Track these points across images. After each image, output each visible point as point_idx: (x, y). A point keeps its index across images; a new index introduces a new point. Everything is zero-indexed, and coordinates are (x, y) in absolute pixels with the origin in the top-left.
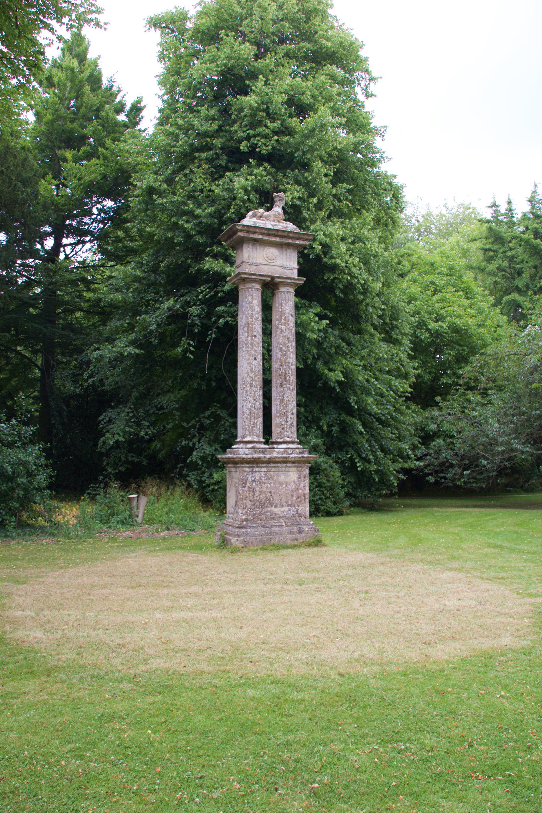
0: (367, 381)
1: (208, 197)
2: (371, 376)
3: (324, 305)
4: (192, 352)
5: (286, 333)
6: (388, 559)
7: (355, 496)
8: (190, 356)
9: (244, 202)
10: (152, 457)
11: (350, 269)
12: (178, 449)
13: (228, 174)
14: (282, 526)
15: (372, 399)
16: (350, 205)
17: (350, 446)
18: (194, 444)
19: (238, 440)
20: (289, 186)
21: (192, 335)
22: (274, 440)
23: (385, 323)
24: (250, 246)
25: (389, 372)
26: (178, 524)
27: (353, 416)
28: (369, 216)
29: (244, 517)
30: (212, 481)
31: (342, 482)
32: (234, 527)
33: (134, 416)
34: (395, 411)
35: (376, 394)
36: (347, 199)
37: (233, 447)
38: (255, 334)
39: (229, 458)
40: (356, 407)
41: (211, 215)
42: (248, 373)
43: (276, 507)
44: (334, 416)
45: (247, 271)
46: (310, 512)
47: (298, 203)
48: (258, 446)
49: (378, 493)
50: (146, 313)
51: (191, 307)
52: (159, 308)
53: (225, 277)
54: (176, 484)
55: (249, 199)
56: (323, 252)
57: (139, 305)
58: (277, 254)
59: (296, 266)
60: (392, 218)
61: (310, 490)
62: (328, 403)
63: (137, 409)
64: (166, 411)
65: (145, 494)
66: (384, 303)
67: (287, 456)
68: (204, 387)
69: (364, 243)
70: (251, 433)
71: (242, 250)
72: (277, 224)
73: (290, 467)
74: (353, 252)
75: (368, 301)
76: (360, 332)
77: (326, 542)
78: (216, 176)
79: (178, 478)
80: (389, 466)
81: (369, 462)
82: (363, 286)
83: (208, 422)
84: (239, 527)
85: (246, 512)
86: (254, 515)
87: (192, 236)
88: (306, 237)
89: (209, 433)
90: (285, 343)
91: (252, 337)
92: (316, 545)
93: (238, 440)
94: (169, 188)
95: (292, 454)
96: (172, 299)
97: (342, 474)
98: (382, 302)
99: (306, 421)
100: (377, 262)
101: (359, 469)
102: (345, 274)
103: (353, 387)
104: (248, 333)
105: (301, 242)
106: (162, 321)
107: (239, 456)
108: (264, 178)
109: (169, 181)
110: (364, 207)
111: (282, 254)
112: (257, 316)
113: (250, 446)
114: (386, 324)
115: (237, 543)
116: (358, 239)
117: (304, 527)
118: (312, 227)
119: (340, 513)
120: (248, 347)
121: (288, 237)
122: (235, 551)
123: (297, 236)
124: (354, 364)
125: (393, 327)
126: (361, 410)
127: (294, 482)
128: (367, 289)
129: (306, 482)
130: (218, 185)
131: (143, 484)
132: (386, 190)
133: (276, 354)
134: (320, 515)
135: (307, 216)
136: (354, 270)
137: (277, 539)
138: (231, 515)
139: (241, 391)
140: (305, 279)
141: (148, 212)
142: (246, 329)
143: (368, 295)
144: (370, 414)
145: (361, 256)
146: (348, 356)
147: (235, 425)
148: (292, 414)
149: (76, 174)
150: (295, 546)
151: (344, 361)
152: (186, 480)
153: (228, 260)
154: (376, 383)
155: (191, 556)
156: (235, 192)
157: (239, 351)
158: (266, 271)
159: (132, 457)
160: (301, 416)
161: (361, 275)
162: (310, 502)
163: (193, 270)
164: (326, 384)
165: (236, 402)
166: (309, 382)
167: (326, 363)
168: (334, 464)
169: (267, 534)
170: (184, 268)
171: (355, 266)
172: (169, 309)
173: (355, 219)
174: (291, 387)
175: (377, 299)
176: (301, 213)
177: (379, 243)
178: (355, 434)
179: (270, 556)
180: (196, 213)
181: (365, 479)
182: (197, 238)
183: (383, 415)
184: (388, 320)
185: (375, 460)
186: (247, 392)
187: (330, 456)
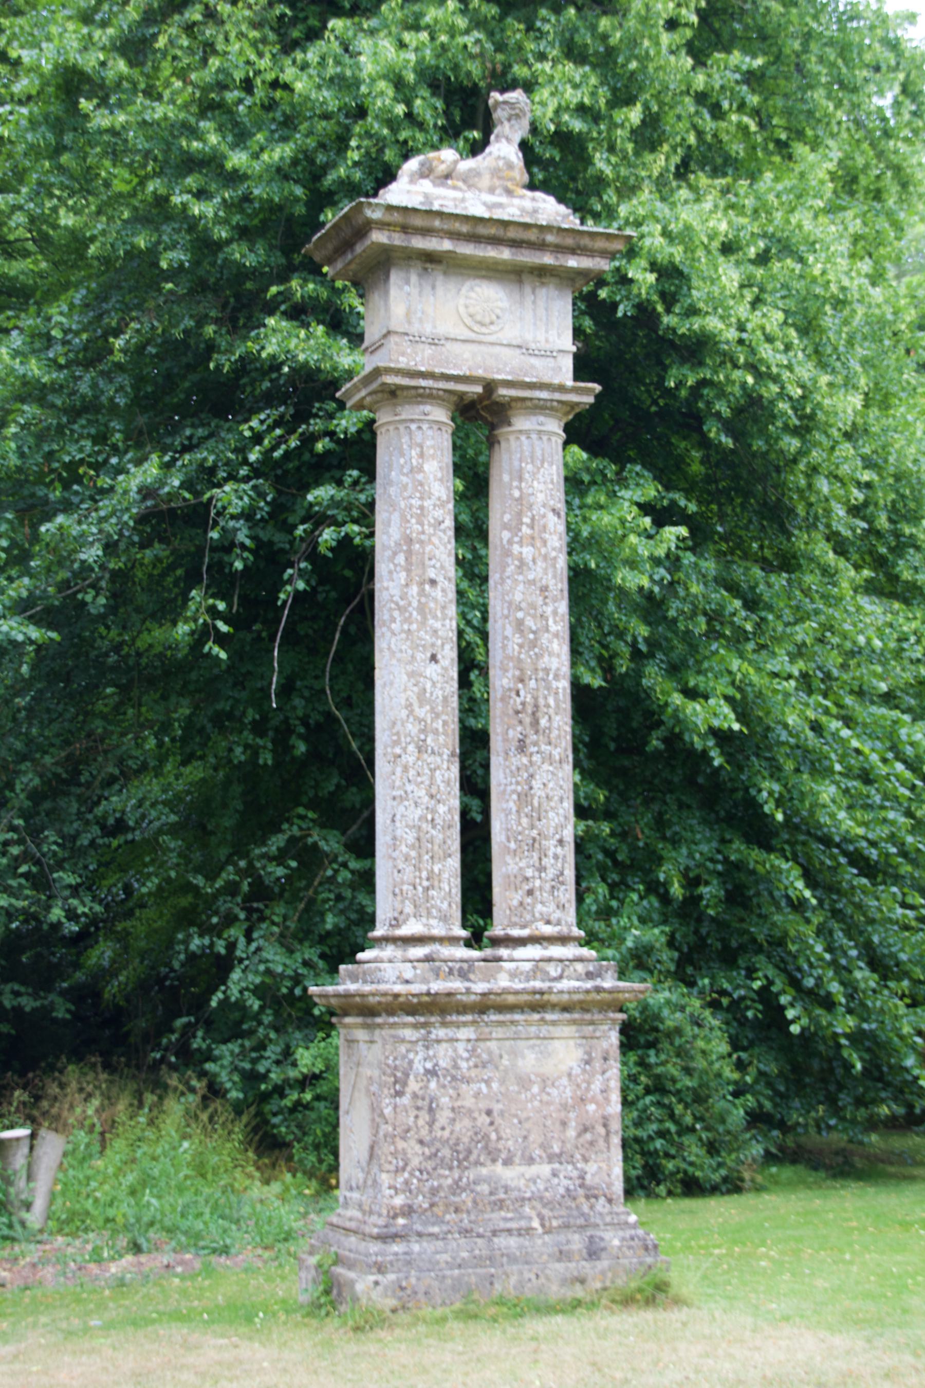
0: (817, 727)
1: (270, 106)
2: (827, 712)
3: (668, 472)
4: (221, 639)
5: (537, 572)
6: (909, 1358)
7: (782, 1125)
8: (216, 649)
9: (392, 124)
10: (86, 995)
11: (753, 351)
12: (176, 965)
13: (336, 24)
14: (529, 1230)
15: (833, 789)
16: (753, 127)
17: (760, 950)
18: (231, 946)
20: (547, 66)
21: (223, 582)
23: (873, 531)
24: (414, 278)
25: (888, 699)
26: (170, 1231)
27: (770, 849)
28: (818, 164)
29: (399, 1201)
30: (293, 1074)
31: (736, 1076)
32: (364, 1236)
33: (25, 857)
34: (912, 831)
35: (847, 774)
36: (742, 107)
37: (360, 956)
38: (432, 573)
39: (348, 995)
40: (780, 817)
41: (281, 173)
42: (409, 706)
43: (507, 1162)
44: (705, 848)
45: (403, 362)
46: (627, 1179)
47: (577, 125)
48: (446, 951)
49: (862, 1114)
50: (67, 507)
51: (219, 485)
52: (112, 489)
53: (335, 384)
54: (166, 1087)
55: (409, 115)
56: (663, 295)
57: (40, 479)
59: (567, 343)
60: (897, 169)
61: (625, 1103)
62: (681, 806)
63: (35, 833)
64: (138, 836)
65: (59, 1125)
66: (869, 464)
67: (544, 985)
68: (266, 758)
69: (801, 260)
70: (422, 909)
71: (387, 292)
72: (504, 199)
73: (554, 1023)
74: (762, 290)
75: (816, 455)
76: (788, 563)
77: (685, 1291)
78: (296, 34)
79: (173, 1068)
80: (896, 1018)
81: (828, 1003)
82: (797, 405)
83: (280, 871)
84: (383, 1238)
85: (407, 1182)
86: (434, 1191)
87: (219, 245)
88: (600, 244)
89: (280, 909)
90: (533, 606)
91: (421, 584)
92: (650, 1302)
93: (378, 932)
94: (135, 73)
95: (561, 977)
96: (154, 457)
97: (735, 1045)
98: (864, 458)
99: (608, 866)
100: (846, 322)
101: (795, 1029)
102: (736, 366)
103: (769, 748)
104: (408, 571)
106: (120, 534)
107: (383, 987)
108: (461, 40)
109: (135, 47)
110: (800, 135)
111: (522, 295)
112: (438, 513)
113: (418, 952)
114: (878, 534)
115: (374, 1295)
116: (781, 246)
117: (607, 1235)
118: (623, 210)
119: (732, 1185)
120: (408, 620)
121: (541, 246)
122: (367, 1324)
123: (569, 241)
124: (771, 672)
125: (902, 545)
126: (797, 828)
127: (571, 1076)
128: (812, 417)
129: (613, 1075)
130: (304, 67)
131: (54, 1089)
132: (877, 69)
133: (503, 645)
134: (662, 1189)
135: (608, 171)
136: (766, 352)
137: (513, 1280)
138: (355, 1195)
140: (597, 388)
141: (65, 159)
142: (401, 559)
143: (817, 436)
144: (827, 841)
145: (791, 304)
146: (750, 646)
147: (366, 881)
148: (561, 842)
150: (577, 1304)
151: (735, 664)
152: (202, 1074)
153: (343, 325)
154: (845, 733)
155: (215, 1347)
156: (364, 89)
157: (379, 632)
159: (17, 994)
160: (591, 849)
161: (790, 368)
162: (625, 1144)
163: (223, 362)
164: (674, 740)
165: (370, 802)
166: (614, 731)
167: (674, 670)
168: (707, 1013)
169: (478, 1261)
170: (192, 353)
171: (769, 339)
172: (146, 492)
173: (768, 175)
174: (556, 753)
175: (846, 449)
176: (588, 161)
177: (852, 256)
178: (779, 908)
179: (490, 1340)
180: (229, 165)
181: (816, 1064)
182: (240, 254)
183: (873, 844)
184: (883, 522)
185: (850, 997)
186: (406, 769)
187: (691, 984)
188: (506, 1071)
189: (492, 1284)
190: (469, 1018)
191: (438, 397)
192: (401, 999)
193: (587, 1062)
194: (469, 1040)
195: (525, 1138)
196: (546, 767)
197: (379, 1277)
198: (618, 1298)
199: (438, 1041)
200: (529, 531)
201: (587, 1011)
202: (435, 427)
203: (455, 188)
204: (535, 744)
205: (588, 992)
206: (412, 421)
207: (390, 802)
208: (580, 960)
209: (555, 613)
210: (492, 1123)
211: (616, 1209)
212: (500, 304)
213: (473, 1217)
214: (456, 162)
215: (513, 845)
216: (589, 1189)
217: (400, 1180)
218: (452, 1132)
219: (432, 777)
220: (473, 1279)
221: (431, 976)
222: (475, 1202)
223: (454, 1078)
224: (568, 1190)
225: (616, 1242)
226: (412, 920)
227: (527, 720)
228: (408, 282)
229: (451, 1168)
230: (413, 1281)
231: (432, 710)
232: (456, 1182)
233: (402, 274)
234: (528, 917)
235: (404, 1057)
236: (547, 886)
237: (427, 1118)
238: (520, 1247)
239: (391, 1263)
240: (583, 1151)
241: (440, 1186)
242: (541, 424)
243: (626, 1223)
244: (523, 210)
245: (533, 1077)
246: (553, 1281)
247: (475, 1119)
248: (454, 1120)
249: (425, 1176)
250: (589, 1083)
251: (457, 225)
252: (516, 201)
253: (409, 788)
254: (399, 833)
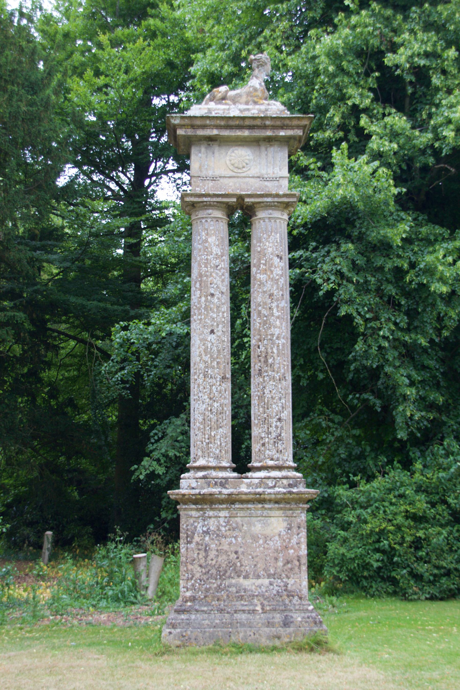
14: (254, 611)
24: (203, 150)
29: (188, 594)
38: (212, 291)
47: (422, 62)
58: (251, 157)
70: (206, 453)
73: (270, 509)
77: (336, 646)
85: (193, 585)
86: (207, 590)
88: (295, 122)
90: (265, 303)
91: (206, 296)
95: (275, 486)
104: (201, 290)
105: (290, 133)
111: (260, 152)
113: (200, 474)
117: (295, 615)
121: (265, 127)
123: (278, 123)
137: (241, 635)
149: (121, 65)
150: (274, 649)
158: (233, 187)
169: (224, 625)
188: (245, 532)
189: (230, 636)
190: (224, 506)
191: (214, 206)
192: (186, 497)
193: (289, 529)
194: (226, 517)
195: (255, 565)
196: (271, 383)
197: (172, 630)
198: (296, 647)
199: (210, 517)
200: (264, 267)
201: (289, 503)
202: (215, 220)
203: (226, 104)
204: (266, 372)
205: (284, 494)
206: (203, 218)
210: (238, 558)
211: (303, 603)
212: (247, 157)
213: (226, 603)
214: (227, 92)
216: (290, 592)
217: (190, 584)
218: (217, 562)
220: (220, 634)
222: (228, 596)
223: (218, 535)
224: (278, 592)
225: (299, 619)
226: (201, 458)
227: (262, 360)
228: (200, 152)
229: (216, 579)
230: (189, 633)
231: (211, 357)
232: (219, 586)
233: (198, 148)
234: (262, 457)
236: (272, 442)
237: (204, 554)
238: (247, 619)
239: (179, 623)
240: (286, 573)
241: (210, 587)
242: (271, 214)
243: (307, 610)
244: (260, 111)
245: (260, 536)
246: (263, 637)
247: (229, 555)
248: (218, 556)
249: (203, 583)
250: (290, 539)
251: (218, 122)
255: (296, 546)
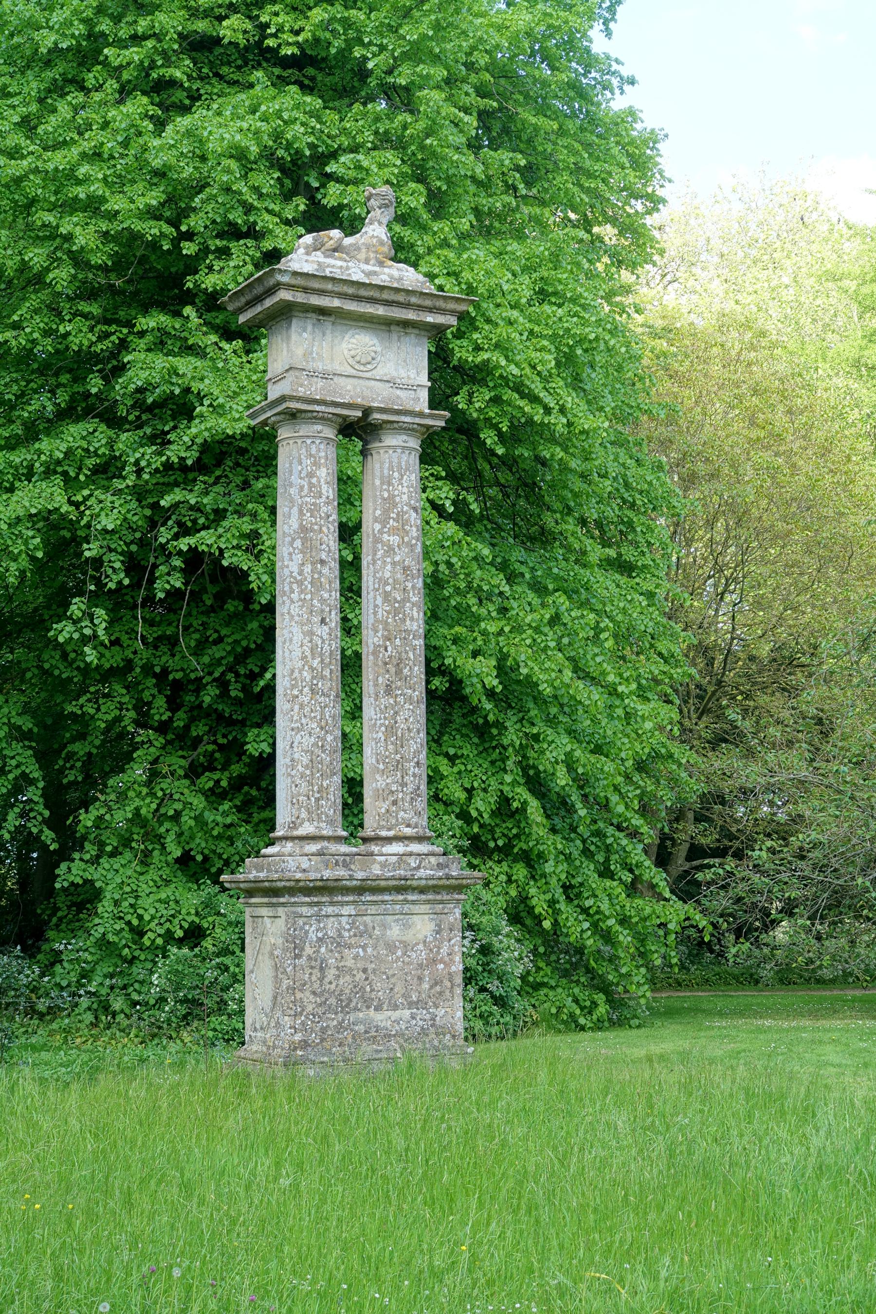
19: (279, 833)
22: (368, 832)
24: (310, 328)
29: (298, 1037)
38: (324, 556)
43: (378, 1009)
45: (301, 392)
48: (334, 847)
71: (289, 338)
72: (377, 269)
73: (413, 902)
76: (542, 538)
86: (324, 1030)
88: (451, 306)
93: (279, 833)
95: (419, 867)
113: (313, 847)
121: (407, 306)
139: (288, 706)
140: (447, 414)
142: (298, 543)
186: (302, 706)
190: (351, 898)
196: (407, 706)
199: (328, 916)
203: (341, 259)
205: (440, 879)
207: (289, 733)
208: (433, 854)
209: (413, 587)
210: (367, 979)
214: (341, 239)
215: (381, 766)
219: (322, 713)
221: (321, 866)
222: (353, 1037)
226: (307, 824)
227: (393, 670)
231: (322, 661)
232: (340, 1024)
233: (301, 324)
235: (302, 929)
236: (408, 798)
244: (391, 277)
252: (386, 270)
253: (304, 721)
254: (296, 756)
255: (447, 959)
